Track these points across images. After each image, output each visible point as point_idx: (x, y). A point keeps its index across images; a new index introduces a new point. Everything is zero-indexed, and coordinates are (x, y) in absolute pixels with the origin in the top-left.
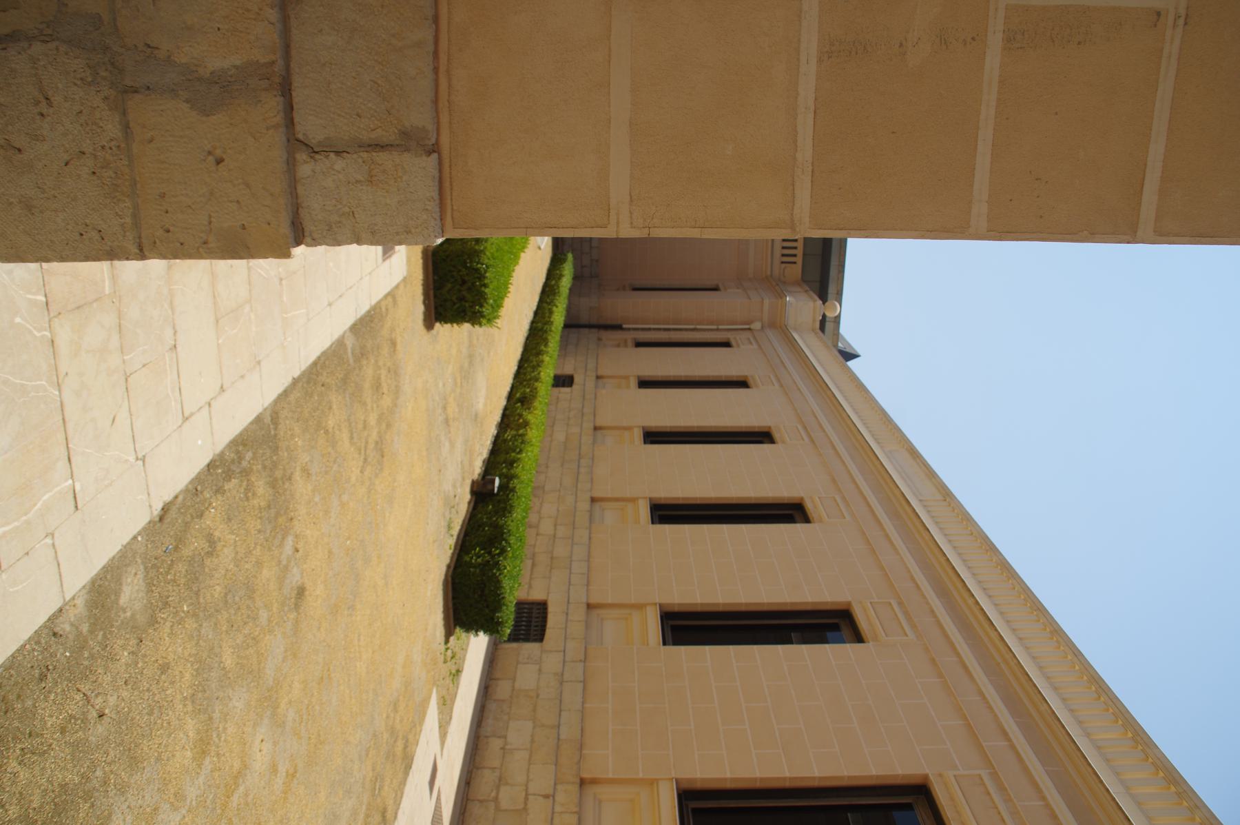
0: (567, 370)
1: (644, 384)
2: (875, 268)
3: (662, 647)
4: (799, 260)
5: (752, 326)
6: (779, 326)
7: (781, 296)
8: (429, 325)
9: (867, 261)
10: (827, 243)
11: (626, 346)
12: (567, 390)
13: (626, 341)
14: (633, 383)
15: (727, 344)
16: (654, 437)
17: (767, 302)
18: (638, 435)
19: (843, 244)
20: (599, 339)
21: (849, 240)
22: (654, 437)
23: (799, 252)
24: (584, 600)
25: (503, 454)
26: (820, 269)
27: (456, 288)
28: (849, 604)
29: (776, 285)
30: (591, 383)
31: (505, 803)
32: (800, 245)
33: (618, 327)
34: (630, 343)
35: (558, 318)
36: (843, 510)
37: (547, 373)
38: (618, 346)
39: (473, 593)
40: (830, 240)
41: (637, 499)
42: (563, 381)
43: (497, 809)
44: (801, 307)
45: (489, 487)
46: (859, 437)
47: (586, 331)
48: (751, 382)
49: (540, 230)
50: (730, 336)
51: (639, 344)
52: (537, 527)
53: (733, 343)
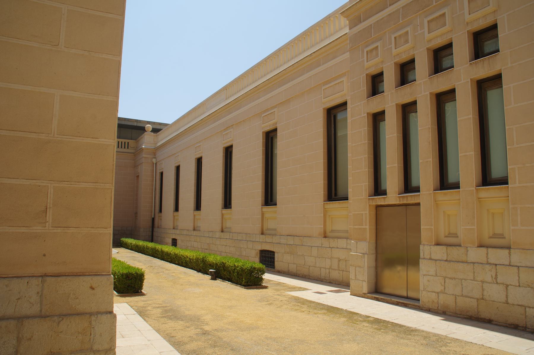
0: (170, 241)
1: (177, 209)
2: (134, 104)
3: (510, 185)
4: (127, 141)
5: (155, 162)
6: (155, 152)
7: (142, 149)
8: (143, 294)
9: (129, 109)
10: (120, 126)
11: (161, 216)
12: (276, 255)
13: (159, 216)
14: (176, 213)
15: (162, 174)
16: (198, 207)
17: (144, 156)
18: (197, 212)
19: (120, 119)
20: (158, 227)
21: (119, 116)
22: (198, 207)
23: (123, 141)
24: (512, 251)
25: (201, 266)
26: (131, 130)
27: (130, 284)
28: (324, 109)
29: (138, 151)
30: (178, 232)
31: (439, 288)
32: (120, 140)
33: (153, 219)
34: (160, 215)
35: (150, 245)
36: (269, 113)
37: (168, 249)
38: (161, 219)
39: (250, 280)
40: (118, 124)
41: (262, 211)
42: (174, 243)
43: (443, 292)
44: (148, 141)
45: (213, 273)
46: (219, 111)
47: (154, 233)
48: (177, 165)
49: (110, 252)
50: (159, 172)
51: (161, 211)
52: (456, 296)
53: (161, 171)
